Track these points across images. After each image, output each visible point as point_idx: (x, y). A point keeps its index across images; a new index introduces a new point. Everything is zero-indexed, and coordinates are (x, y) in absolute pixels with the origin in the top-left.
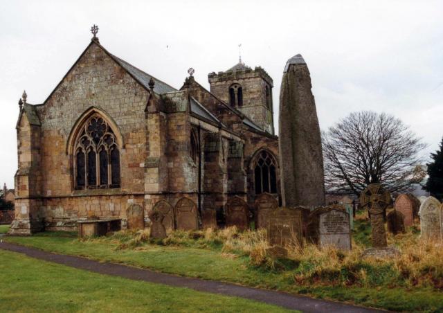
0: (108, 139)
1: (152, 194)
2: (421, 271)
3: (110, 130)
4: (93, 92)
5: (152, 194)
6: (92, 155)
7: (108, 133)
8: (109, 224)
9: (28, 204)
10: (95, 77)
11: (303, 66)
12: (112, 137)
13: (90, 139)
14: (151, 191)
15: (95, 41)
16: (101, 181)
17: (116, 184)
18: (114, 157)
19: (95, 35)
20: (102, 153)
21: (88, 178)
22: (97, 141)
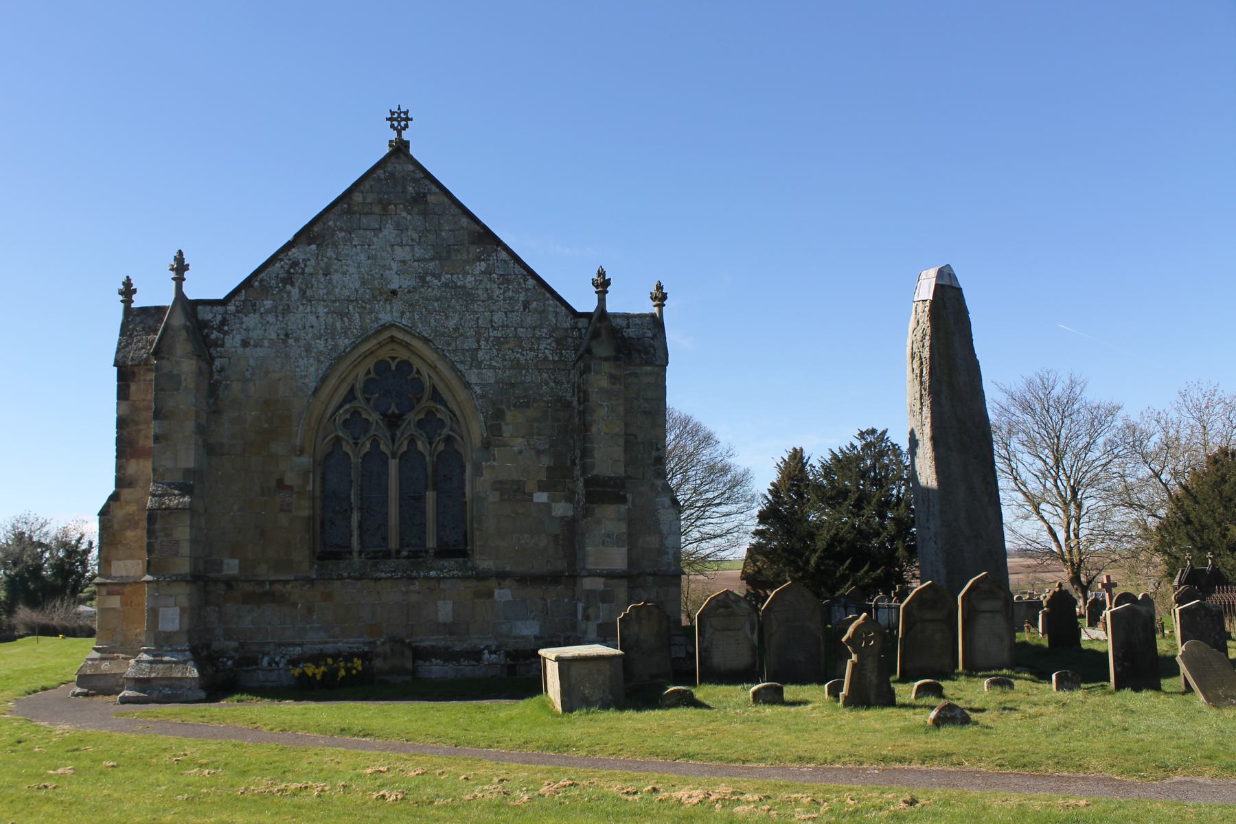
0: (429, 423)
1: (525, 580)
2: (1208, 457)
3: (436, 396)
4: (394, 286)
5: (525, 580)
6: (375, 458)
7: (431, 404)
8: (593, 636)
9: (184, 601)
10: (401, 245)
11: (952, 277)
12: (442, 414)
13: (374, 417)
14: (605, 566)
15: (400, 149)
16: (402, 539)
17: (456, 549)
18: (447, 472)
19: (399, 134)
20: (409, 458)
21: (360, 526)
22: (393, 422)
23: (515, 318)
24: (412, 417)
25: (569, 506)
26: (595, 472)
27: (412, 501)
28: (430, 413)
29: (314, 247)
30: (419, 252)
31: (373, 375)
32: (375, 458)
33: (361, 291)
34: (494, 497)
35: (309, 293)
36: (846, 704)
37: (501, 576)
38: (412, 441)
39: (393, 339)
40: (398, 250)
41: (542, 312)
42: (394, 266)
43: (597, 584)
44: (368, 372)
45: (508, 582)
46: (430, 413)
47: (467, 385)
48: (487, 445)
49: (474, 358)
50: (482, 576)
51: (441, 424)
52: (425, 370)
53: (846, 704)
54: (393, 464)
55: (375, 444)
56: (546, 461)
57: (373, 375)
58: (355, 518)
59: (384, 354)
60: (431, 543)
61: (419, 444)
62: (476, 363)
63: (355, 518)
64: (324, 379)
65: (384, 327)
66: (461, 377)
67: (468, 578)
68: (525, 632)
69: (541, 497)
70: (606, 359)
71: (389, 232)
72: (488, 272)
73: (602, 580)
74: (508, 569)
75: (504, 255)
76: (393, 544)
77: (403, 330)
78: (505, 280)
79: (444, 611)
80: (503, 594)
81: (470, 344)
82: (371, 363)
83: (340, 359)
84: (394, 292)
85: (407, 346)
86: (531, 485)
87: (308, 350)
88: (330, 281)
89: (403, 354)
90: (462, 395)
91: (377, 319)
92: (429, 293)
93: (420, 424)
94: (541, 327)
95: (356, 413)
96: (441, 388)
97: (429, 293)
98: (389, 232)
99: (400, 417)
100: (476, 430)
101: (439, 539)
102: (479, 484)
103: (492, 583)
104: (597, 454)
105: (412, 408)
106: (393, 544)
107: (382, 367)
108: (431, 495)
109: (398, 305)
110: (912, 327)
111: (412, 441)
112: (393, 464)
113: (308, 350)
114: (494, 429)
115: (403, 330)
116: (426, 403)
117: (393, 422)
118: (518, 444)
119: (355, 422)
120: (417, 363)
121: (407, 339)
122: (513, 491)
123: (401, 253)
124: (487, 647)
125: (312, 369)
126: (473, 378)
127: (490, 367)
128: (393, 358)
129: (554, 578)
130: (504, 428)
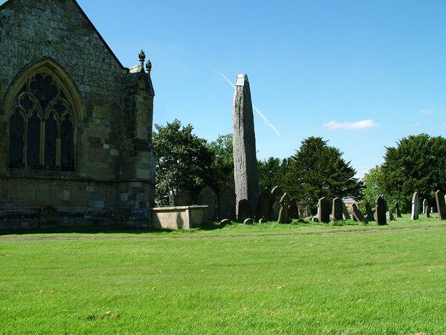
0: (60, 108)
1: (98, 183)
3: (63, 95)
4: (50, 39)
6: (35, 121)
17: (70, 165)
20: (50, 123)
23: (99, 65)
24: (52, 102)
25: (117, 151)
26: (137, 137)
27: (50, 145)
28: (59, 102)
29: (13, 11)
30: (61, 26)
31: (35, 80)
32: (35, 121)
33: (35, 38)
34: (88, 144)
35: (10, 33)
36: (280, 223)
37: (90, 180)
38: (51, 114)
39: (47, 65)
40: (52, 23)
41: (110, 65)
42: (50, 29)
43: (139, 185)
44: (33, 78)
45: (92, 184)
46: (59, 102)
47: (79, 92)
48: (86, 120)
49: (82, 80)
50: (82, 180)
51: (64, 108)
52: (59, 81)
53: (280, 223)
54: (43, 124)
55: (35, 113)
56: (109, 130)
57: (35, 80)
58: (26, 148)
59: (40, 71)
60: (58, 163)
61: (54, 116)
62: (83, 83)
63: (26, 148)
64: (17, 77)
65: (46, 58)
66: (77, 88)
67: (75, 180)
68: (99, 206)
69: (106, 146)
70: (143, 90)
71: (48, 12)
72: (90, 41)
73: (141, 183)
74: (92, 177)
75: (96, 35)
76: (42, 162)
77: (53, 61)
78: (96, 47)
79: (66, 195)
80: (90, 189)
81: (81, 73)
82: (34, 74)
83: (23, 70)
84: (50, 42)
85: (53, 69)
86: (103, 141)
87: (9, 62)
88: (21, 30)
89: (50, 72)
90: (77, 96)
91: (42, 53)
92: (65, 46)
93: (55, 107)
94: (109, 70)
95: (26, 97)
96: (65, 91)
97: (65, 46)
98: (48, 12)
99: (47, 102)
100: (82, 112)
101: (62, 162)
102: (82, 138)
103: (86, 183)
104: (138, 129)
105: (52, 99)
106: (42, 162)
107: (39, 76)
108: (59, 141)
109: (51, 49)
110: (234, 95)
111: (51, 114)
112: (43, 124)
113: (9, 62)
114: (89, 114)
115: (53, 61)
116: (58, 97)
117: (44, 104)
118: (98, 121)
119: (26, 102)
120: (55, 77)
121: (55, 65)
122: (96, 142)
123: (53, 24)
124: (84, 212)
125: (11, 72)
126: (81, 89)
127: (89, 85)
128: (44, 74)
129: (110, 183)
130: (93, 114)
